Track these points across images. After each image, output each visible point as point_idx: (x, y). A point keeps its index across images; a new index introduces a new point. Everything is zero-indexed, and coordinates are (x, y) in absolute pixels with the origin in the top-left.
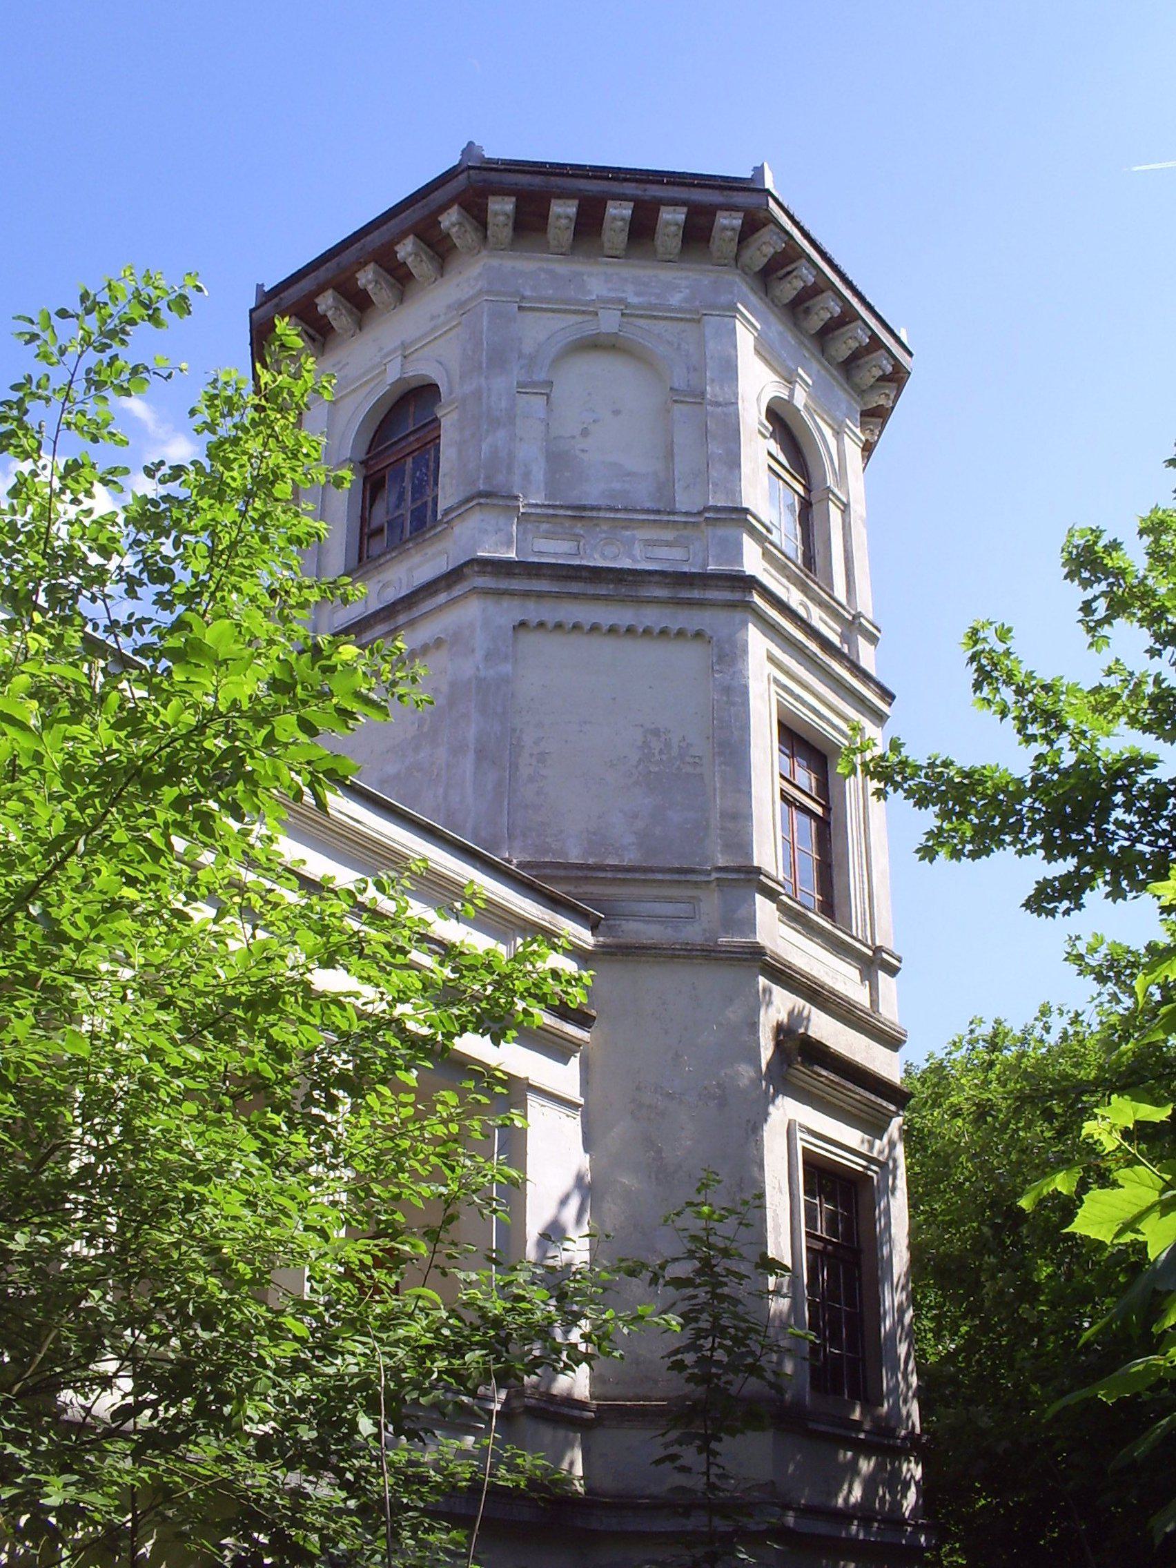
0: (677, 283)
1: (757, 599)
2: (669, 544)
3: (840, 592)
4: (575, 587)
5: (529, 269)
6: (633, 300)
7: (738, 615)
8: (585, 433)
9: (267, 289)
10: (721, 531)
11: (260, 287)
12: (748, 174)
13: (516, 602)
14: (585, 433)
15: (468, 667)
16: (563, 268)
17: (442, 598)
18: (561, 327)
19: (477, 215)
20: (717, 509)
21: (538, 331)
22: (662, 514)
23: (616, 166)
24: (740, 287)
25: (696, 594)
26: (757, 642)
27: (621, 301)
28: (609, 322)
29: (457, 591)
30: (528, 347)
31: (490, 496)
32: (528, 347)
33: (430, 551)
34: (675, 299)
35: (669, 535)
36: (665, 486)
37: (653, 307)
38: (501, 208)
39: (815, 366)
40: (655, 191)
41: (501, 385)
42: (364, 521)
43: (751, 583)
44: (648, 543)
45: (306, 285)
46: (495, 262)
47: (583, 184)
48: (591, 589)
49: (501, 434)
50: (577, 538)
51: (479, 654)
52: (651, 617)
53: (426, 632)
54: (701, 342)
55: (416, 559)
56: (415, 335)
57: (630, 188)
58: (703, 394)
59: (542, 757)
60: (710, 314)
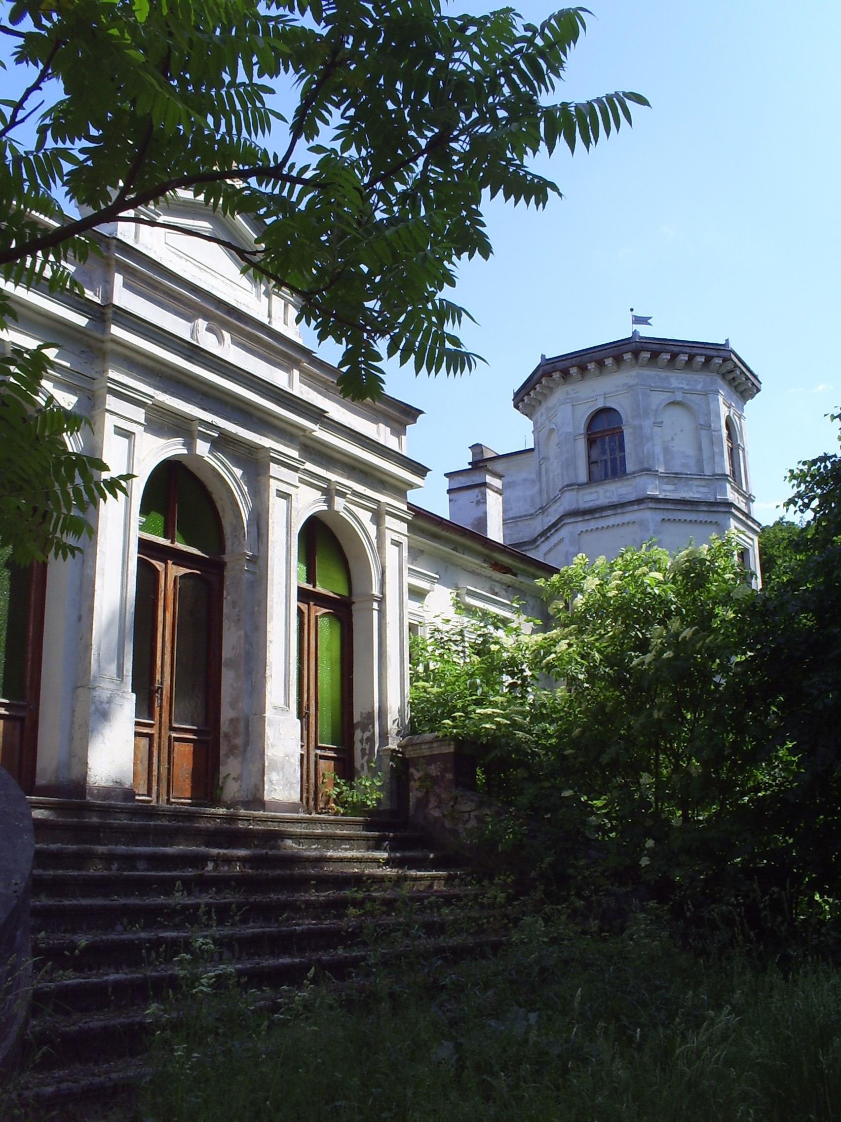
0: (699, 380)
1: (733, 510)
2: (704, 487)
3: (744, 489)
4: (679, 507)
5: (650, 373)
6: (686, 387)
7: (727, 515)
8: (673, 440)
9: (547, 357)
10: (720, 482)
11: (543, 356)
12: (724, 342)
13: (661, 511)
14: (673, 440)
16: (663, 374)
17: (636, 507)
18: (664, 397)
19: (636, 354)
20: (718, 475)
21: (658, 399)
22: (700, 475)
24: (720, 382)
25: (715, 509)
26: (733, 523)
27: (682, 388)
28: (679, 397)
29: (642, 507)
31: (648, 471)
32: (654, 407)
33: (625, 483)
35: (703, 483)
36: (700, 462)
37: (692, 390)
38: (556, 375)
39: (726, 387)
42: (589, 457)
43: (731, 505)
44: (697, 486)
46: (641, 372)
47: (672, 348)
48: (684, 508)
49: (650, 444)
50: (674, 484)
51: (651, 532)
52: (702, 517)
53: (627, 518)
54: (708, 404)
55: (619, 484)
57: (688, 350)
58: (710, 426)
60: (709, 394)
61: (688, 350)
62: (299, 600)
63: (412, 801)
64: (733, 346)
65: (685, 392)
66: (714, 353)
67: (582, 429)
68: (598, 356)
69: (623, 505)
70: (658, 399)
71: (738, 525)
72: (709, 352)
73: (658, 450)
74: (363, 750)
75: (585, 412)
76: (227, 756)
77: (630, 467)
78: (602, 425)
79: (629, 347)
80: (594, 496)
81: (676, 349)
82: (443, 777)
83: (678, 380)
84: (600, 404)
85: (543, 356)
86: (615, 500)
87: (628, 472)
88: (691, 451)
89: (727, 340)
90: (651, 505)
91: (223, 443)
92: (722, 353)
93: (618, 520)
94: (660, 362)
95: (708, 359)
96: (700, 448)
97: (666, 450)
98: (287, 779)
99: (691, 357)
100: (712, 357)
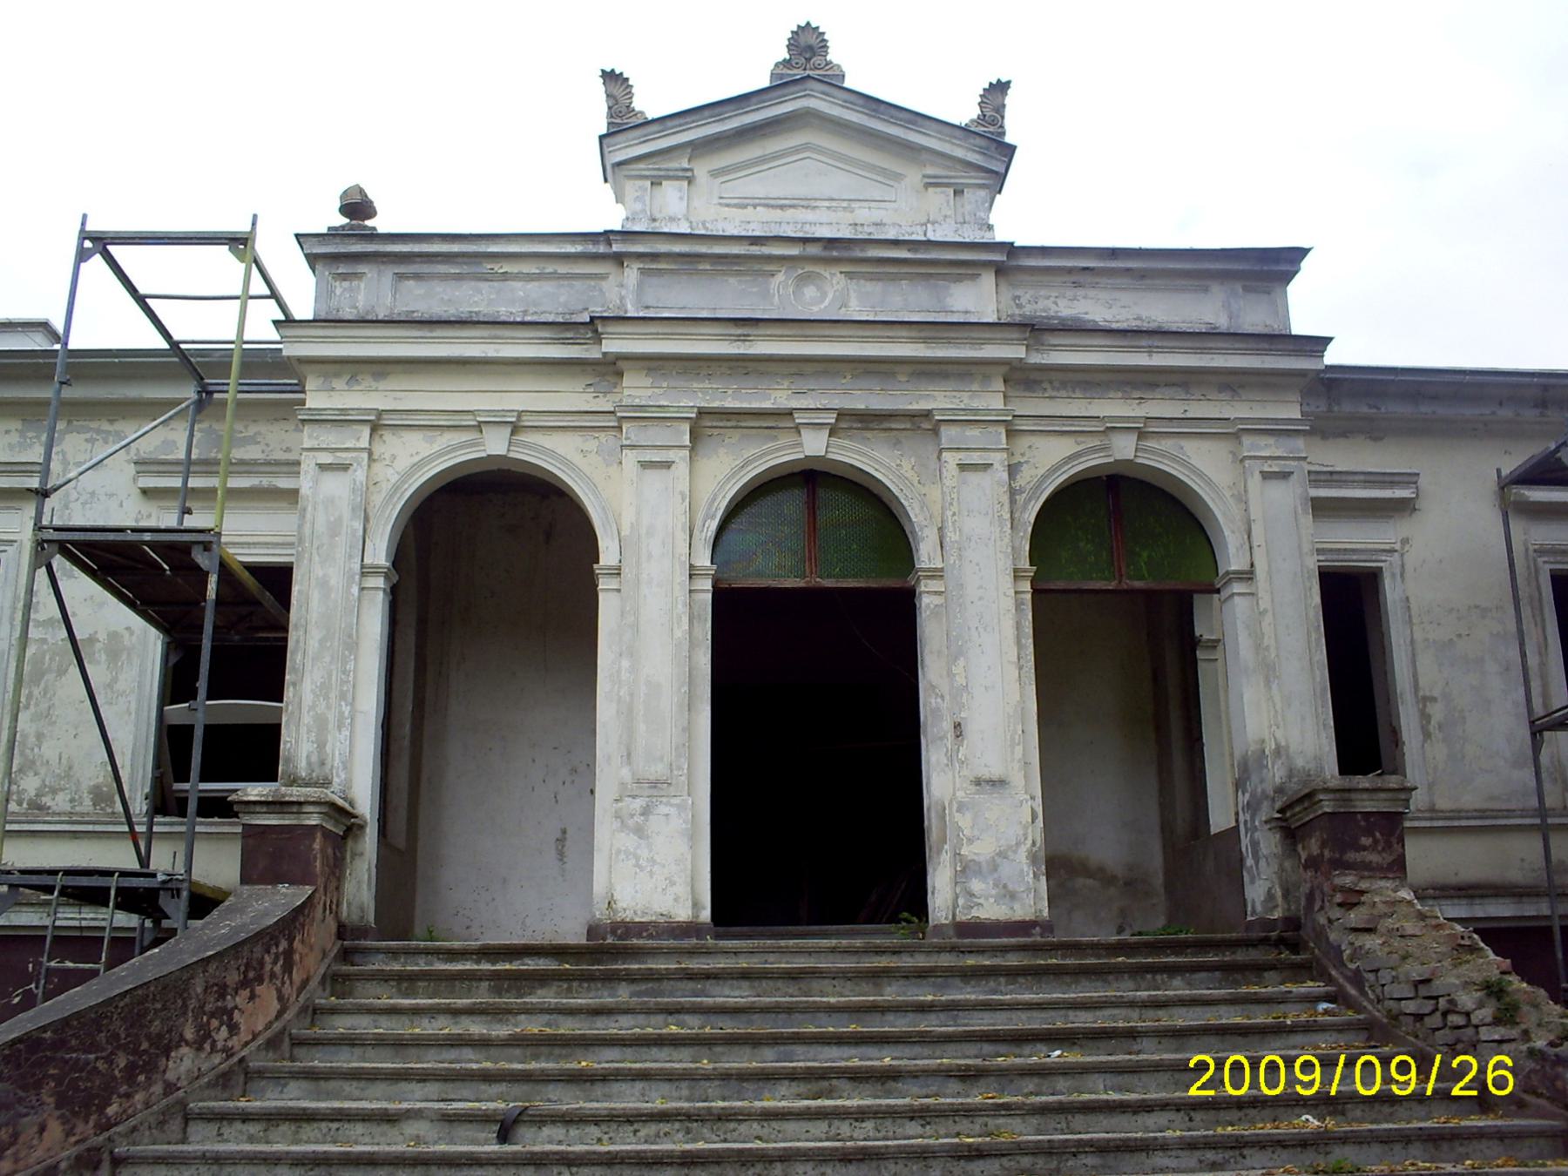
23: (1110, 245)
82: (1322, 855)
98: (1005, 886)
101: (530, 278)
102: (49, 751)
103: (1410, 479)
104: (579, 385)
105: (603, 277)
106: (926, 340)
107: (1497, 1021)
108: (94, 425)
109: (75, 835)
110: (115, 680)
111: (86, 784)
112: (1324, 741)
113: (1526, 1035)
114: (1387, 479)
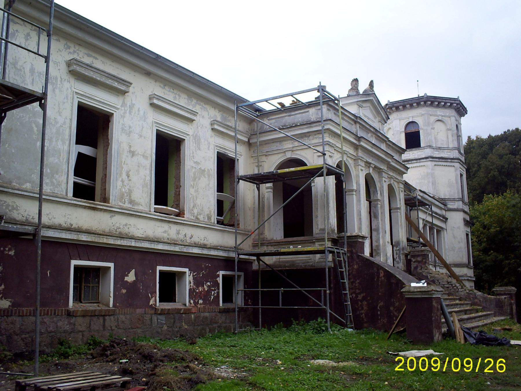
4: (441, 160)
15: (430, 171)
16: (435, 109)
17: (425, 160)
18: (436, 118)
30: (431, 122)
31: (430, 147)
32: (431, 122)
34: (447, 114)
38: (394, 109)
40: (447, 101)
41: (429, 128)
45: (398, 104)
52: (448, 164)
53: (421, 164)
56: (418, 116)
57: (444, 101)
59: (438, 183)
61: (444, 101)
62: (76, 174)
63: (412, 268)
64: (461, 99)
65: (442, 116)
66: (454, 102)
67: (404, 130)
68: (410, 102)
69: (420, 159)
70: (433, 119)
71: (342, 111)
72: (452, 102)
73: (433, 138)
74: (397, 253)
75: (404, 123)
76: (376, 255)
77: (422, 145)
78: (412, 129)
79: (456, 102)
80: (408, 155)
81: (441, 100)
83: (440, 112)
84: (411, 121)
85: (389, 101)
86: (416, 157)
87: (422, 146)
88: (445, 139)
89: (458, 97)
90: (431, 159)
91: (375, 168)
92: (456, 102)
93: (418, 164)
94: (434, 105)
95: (451, 104)
96: (448, 137)
97: (435, 138)
99: (445, 103)
100: (453, 103)
101: (346, 121)
102: (198, 202)
103: (195, 113)
104: (352, 148)
105: (352, 125)
106: (385, 155)
107: (462, 288)
108: (202, 104)
109: (205, 228)
110: (209, 184)
111: (206, 213)
112: (192, 191)
113: (465, 290)
114: (193, 113)
